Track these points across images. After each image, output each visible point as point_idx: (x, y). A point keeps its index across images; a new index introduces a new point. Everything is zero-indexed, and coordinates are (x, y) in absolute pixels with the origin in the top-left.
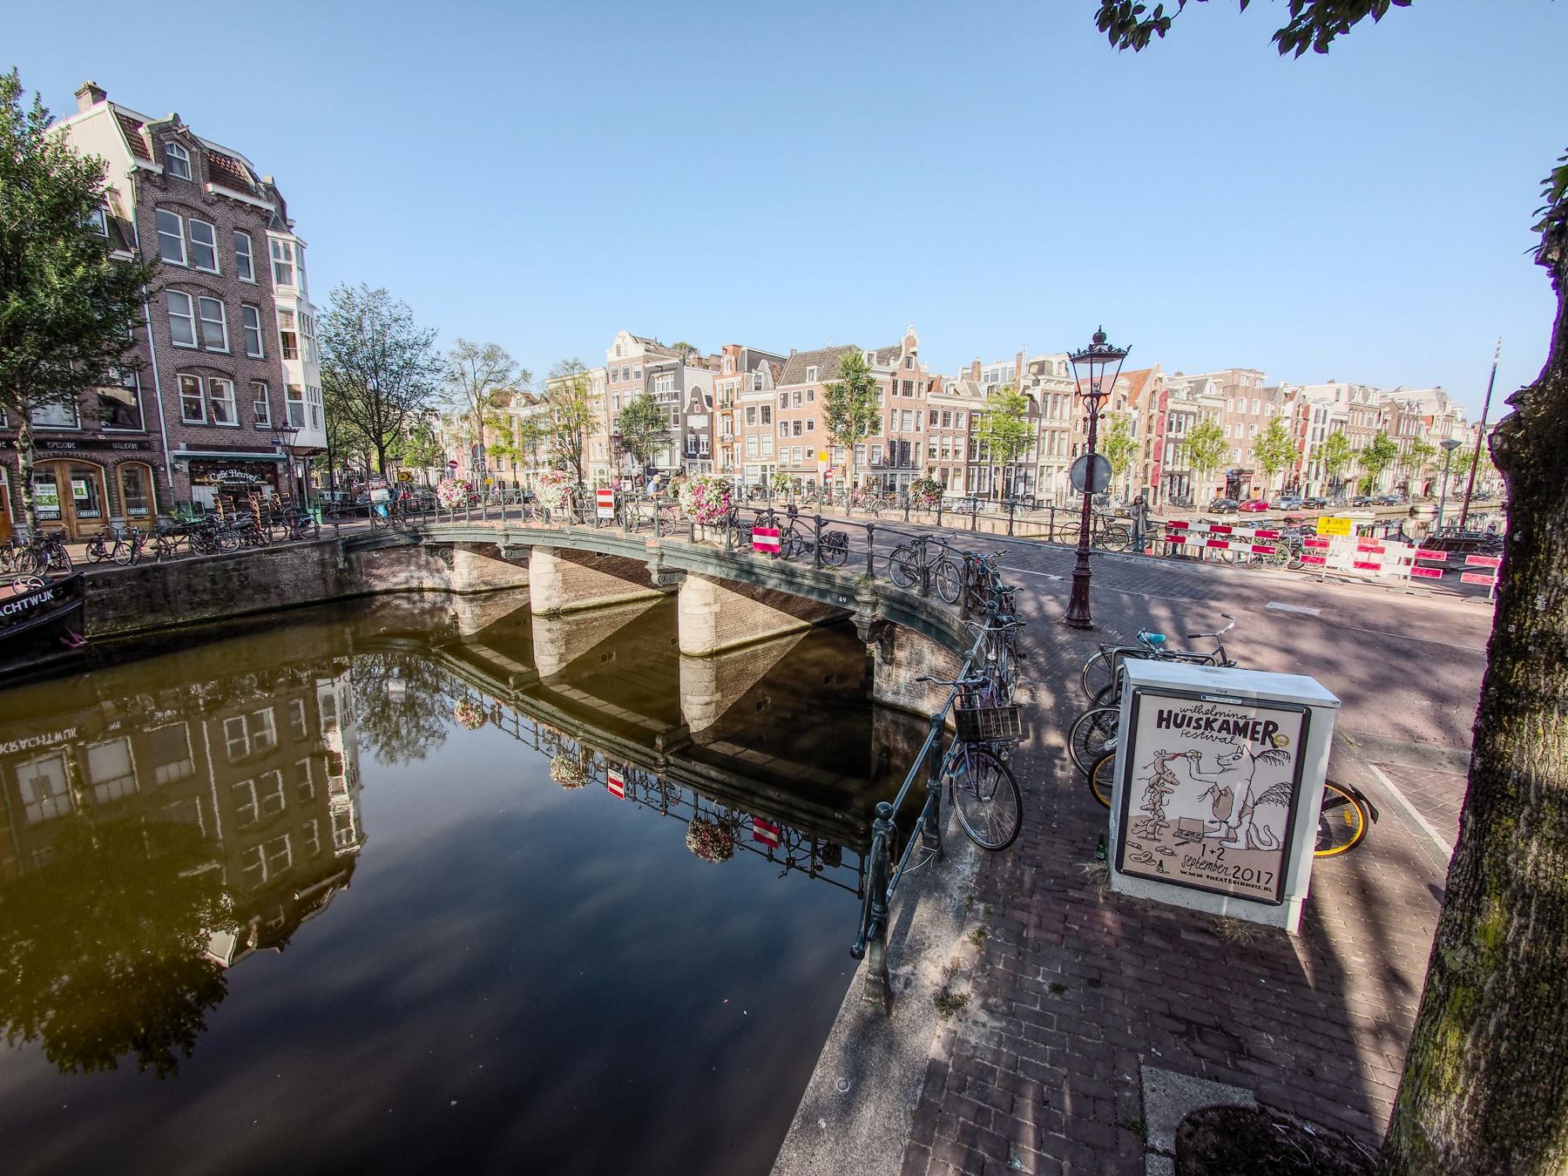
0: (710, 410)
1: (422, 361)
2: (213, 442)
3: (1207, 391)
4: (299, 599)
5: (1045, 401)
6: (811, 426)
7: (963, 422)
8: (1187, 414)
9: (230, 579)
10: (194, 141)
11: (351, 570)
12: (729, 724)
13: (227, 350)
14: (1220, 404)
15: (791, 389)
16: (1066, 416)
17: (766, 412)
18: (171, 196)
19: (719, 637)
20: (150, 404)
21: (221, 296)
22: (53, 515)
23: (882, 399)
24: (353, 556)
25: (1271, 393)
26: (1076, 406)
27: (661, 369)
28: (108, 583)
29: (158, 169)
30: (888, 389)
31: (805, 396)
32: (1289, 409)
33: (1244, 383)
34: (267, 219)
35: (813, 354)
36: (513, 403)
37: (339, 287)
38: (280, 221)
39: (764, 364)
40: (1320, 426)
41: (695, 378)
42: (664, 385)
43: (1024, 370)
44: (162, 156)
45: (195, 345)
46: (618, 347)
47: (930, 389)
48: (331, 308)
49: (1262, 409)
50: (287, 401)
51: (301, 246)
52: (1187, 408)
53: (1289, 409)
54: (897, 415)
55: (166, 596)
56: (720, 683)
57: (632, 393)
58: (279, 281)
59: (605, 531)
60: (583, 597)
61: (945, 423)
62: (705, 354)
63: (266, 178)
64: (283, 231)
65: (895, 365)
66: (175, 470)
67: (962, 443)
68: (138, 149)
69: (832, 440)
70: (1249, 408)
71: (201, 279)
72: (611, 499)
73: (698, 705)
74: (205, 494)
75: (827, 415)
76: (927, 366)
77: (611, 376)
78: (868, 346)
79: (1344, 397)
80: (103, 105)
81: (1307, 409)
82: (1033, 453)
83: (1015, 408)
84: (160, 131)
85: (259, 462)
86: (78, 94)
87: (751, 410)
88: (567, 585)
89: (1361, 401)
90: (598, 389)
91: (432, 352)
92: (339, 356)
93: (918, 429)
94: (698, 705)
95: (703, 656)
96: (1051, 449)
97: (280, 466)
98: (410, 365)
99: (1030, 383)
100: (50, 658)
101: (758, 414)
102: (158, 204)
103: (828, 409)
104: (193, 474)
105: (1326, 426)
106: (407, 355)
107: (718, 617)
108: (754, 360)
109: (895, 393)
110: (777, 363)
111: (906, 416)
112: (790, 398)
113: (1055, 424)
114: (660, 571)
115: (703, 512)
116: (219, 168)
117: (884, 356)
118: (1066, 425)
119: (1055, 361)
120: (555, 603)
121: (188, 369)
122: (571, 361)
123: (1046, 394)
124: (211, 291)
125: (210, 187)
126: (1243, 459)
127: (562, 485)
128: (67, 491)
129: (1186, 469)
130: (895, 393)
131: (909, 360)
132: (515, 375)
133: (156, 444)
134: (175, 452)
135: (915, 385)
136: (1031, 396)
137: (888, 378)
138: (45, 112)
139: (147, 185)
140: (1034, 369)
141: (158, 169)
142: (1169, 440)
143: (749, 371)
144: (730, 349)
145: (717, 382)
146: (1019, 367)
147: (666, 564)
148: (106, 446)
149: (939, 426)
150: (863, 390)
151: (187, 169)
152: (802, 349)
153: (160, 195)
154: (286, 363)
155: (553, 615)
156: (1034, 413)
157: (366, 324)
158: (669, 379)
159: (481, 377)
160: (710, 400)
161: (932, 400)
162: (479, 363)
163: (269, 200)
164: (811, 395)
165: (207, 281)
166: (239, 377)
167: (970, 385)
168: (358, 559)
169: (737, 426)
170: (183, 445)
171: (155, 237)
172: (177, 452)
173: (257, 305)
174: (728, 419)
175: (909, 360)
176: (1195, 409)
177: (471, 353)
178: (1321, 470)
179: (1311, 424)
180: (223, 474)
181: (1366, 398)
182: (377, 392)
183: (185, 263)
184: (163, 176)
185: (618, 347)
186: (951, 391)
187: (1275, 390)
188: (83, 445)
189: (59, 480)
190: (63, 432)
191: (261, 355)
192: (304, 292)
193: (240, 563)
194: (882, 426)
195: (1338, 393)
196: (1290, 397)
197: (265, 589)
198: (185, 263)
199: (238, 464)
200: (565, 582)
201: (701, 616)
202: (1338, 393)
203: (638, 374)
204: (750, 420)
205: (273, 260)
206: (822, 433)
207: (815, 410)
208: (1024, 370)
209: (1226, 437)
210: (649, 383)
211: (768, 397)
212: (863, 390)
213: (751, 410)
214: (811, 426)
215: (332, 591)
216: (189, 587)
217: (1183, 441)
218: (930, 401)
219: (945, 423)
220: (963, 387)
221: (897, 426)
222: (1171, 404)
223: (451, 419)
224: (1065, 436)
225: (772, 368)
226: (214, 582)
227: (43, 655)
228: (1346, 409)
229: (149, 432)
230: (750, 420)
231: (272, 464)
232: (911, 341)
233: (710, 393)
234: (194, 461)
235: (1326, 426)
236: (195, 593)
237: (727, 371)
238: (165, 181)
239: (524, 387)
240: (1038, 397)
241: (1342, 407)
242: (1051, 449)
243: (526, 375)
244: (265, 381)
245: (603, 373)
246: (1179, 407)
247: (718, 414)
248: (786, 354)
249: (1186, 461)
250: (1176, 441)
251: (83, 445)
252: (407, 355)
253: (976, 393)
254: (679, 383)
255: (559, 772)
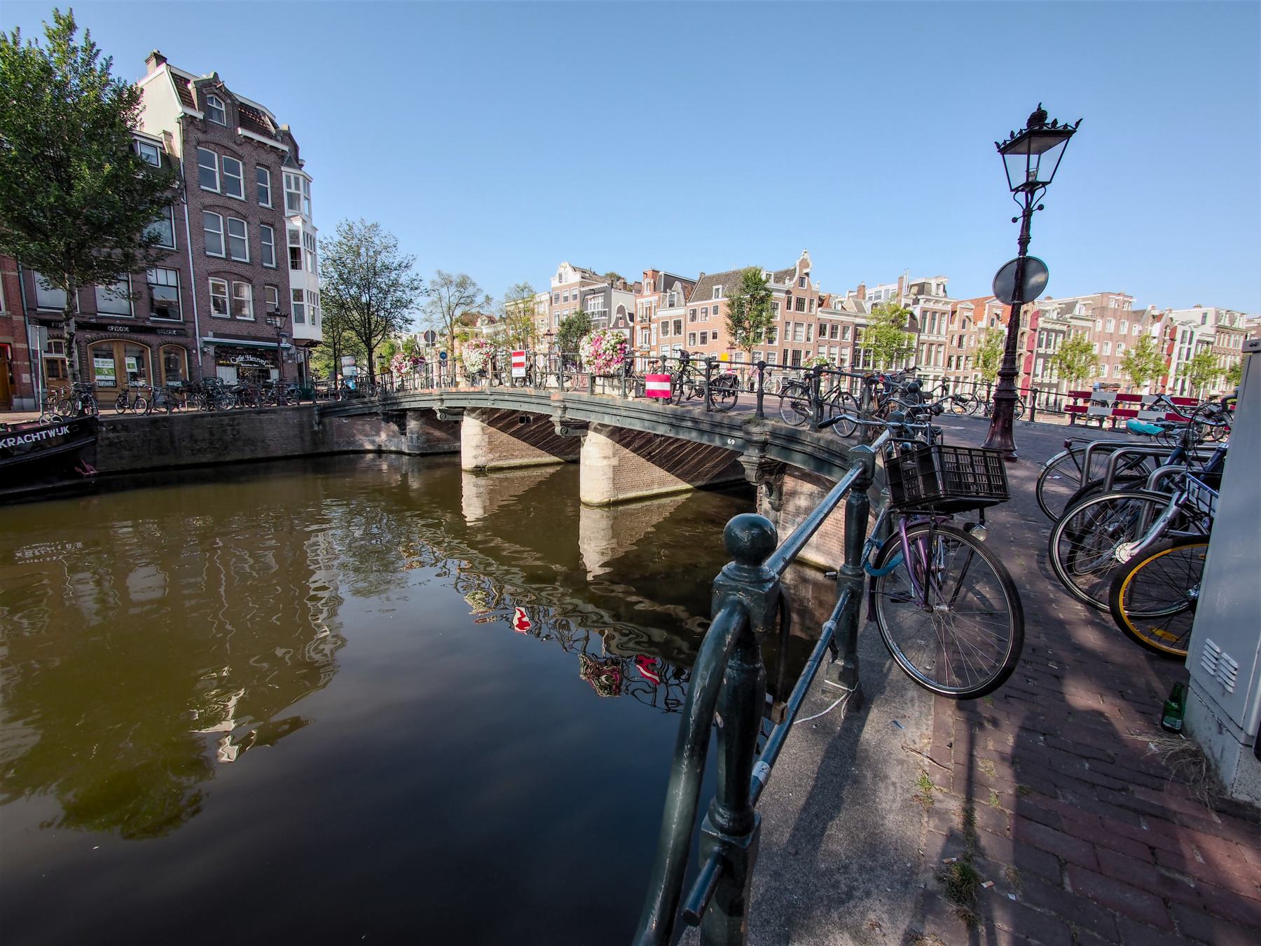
0: (631, 324)
1: (404, 279)
2: (233, 332)
3: (1076, 312)
4: (280, 453)
5: (924, 317)
6: (715, 336)
7: (849, 335)
8: (1057, 332)
9: (225, 432)
10: (228, 94)
11: (324, 431)
12: (623, 568)
13: (247, 260)
14: (1089, 324)
15: (698, 305)
16: (943, 331)
17: (678, 325)
18: (209, 137)
19: (616, 486)
20: (187, 299)
21: (245, 218)
22: (111, 384)
23: (778, 313)
24: (326, 420)
25: (1138, 315)
26: (952, 322)
27: (594, 292)
28: (126, 428)
29: (200, 115)
30: (782, 305)
31: (711, 311)
32: (1156, 329)
33: (1112, 305)
34: (282, 158)
35: (719, 276)
36: (479, 323)
37: (344, 221)
38: (294, 160)
39: (678, 285)
40: (1186, 345)
41: (620, 299)
42: (595, 305)
43: (905, 292)
44: (203, 106)
45: (224, 256)
46: (560, 276)
47: (820, 305)
48: (337, 238)
49: (1130, 329)
50: (292, 302)
51: (308, 181)
52: (1058, 327)
53: (1156, 329)
54: (790, 328)
55: (172, 442)
56: (615, 531)
57: (568, 310)
58: (291, 207)
59: (519, 390)
60: (506, 458)
61: (833, 335)
62: (630, 281)
63: (283, 127)
64: (294, 167)
65: (789, 284)
66: (204, 353)
67: (848, 353)
68: (185, 98)
69: (732, 344)
70: (1117, 327)
71: (230, 204)
72: (522, 359)
73: (594, 547)
74: (227, 376)
75: (729, 322)
76: (817, 285)
77: (554, 299)
78: (768, 267)
79: (1211, 320)
80: (163, 67)
81: (1174, 330)
82: (913, 359)
83: (897, 322)
84: (203, 86)
85: (269, 349)
86: (147, 61)
87: (665, 325)
88: (492, 446)
89: (1227, 324)
90: (543, 309)
91: (411, 273)
92: (341, 275)
93: (808, 339)
94: (594, 547)
95: (601, 506)
96: (929, 357)
97: (285, 354)
98: (395, 284)
99: (910, 302)
100: (66, 483)
101: (671, 328)
102: (199, 143)
103: (730, 317)
104: (218, 356)
105: (1193, 346)
106: (393, 276)
107: (617, 470)
108: (669, 281)
109: (788, 308)
110: (688, 285)
111: (798, 329)
112: (699, 314)
113: (933, 338)
114: (563, 423)
115: (601, 362)
116: (248, 116)
117: (780, 278)
118: (942, 339)
119: (934, 283)
120: (481, 461)
121: (216, 274)
122: (521, 285)
123: (924, 312)
124: (238, 214)
125: (240, 131)
126: (1110, 374)
127: (485, 350)
128: (121, 366)
129: (1055, 380)
130: (788, 308)
131: (802, 280)
132: (480, 299)
133: (190, 332)
134: (205, 338)
135: (807, 302)
136: (912, 315)
137: (783, 295)
138: (93, 45)
139: (191, 128)
140: (915, 290)
141: (200, 115)
142: (1039, 356)
143: (665, 291)
144: (650, 273)
145: (639, 301)
146: (900, 288)
147: (569, 415)
148: (151, 331)
149: (827, 336)
150: (763, 300)
151: (218, 113)
152: (709, 272)
153: (200, 136)
154: (292, 273)
155: (479, 471)
156: (913, 328)
157: (363, 250)
158: (601, 300)
159: (454, 300)
160: (632, 317)
161: (819, 313)
162: (453, 289)
163: (283, 142)
164: (716, 311)
165: (235, 206)
166: (255, 281)
167: (856, 303)
168: (331, 423)
169: (654, 337)
170: (211, 333)
171: (197, 170)
172: (206, 339)
173: (272, 225)
174: (646, 332)
175: (802, 280)
176: (1065, 328)
177: (448, 282)
178: (1187, 386)
179: (1177, 344)
180: (241, 358)
181: (1232, 321)
182: (369, 305)
183: (218, 191)
184: (204, 121)
185: (560, 276)
186: (839, 307)
187: (1143, 312)
188: (135, 329)
189: (116, 356)
190: (120, 319)
191: (274, 265)
192: (309, 216)
193: (233, 420)
194: (777, 335)
195: (1205, 316)
196: (1157, 318)
197: (251, 442)
198: (218, 191)
199: (253, 351)
200: (490, 443)
201: (598, 468)
202: (1205, 316)
203: (575, 297)
204: (665, 333)
205: (285, 190)
206: (725, 338)
207: (720, 322)
208: (905, 292)
209: (1095, 351)
210: (584, 302)
211: (679, 312)
212: (763, 300)
213: (665, 325)
214: (715, 336)
215: (308, 449)
216: (191, 436)
217: (1050, 356)
218: (820, 315)
219: (833, 335)
220: (851, 307)
221: (790, 337)
222: (1041, 323)
223: (420, 321)
224: (941, 349)
225: (684, 288)
226: (212, 434)
227: (60, 480)
228: (1213, 331)
229: (185, 322)
230: (665, 333)
231: (275, 351)
232: (804, 264)
233: (633, 311)
234: (219, 346)
235: (1193, 346)
236: (196, 441)
237: (647, 292)
238: (205, 126)
239: (486, 311)
240: (917, 313)
241: (1209, 328)
242: (929, 357)
243: (488, 299)
244: (276, 286)
245: (547, 297)
246: (1049, 326)
247: (638, 328)
248: (696, 278)
249: (1056, 372)
250: (1046, 357)
251: (135, 329)
252: (393, 276)
253: (861, 309)
254: (607, 303)
255: (474, 604)
